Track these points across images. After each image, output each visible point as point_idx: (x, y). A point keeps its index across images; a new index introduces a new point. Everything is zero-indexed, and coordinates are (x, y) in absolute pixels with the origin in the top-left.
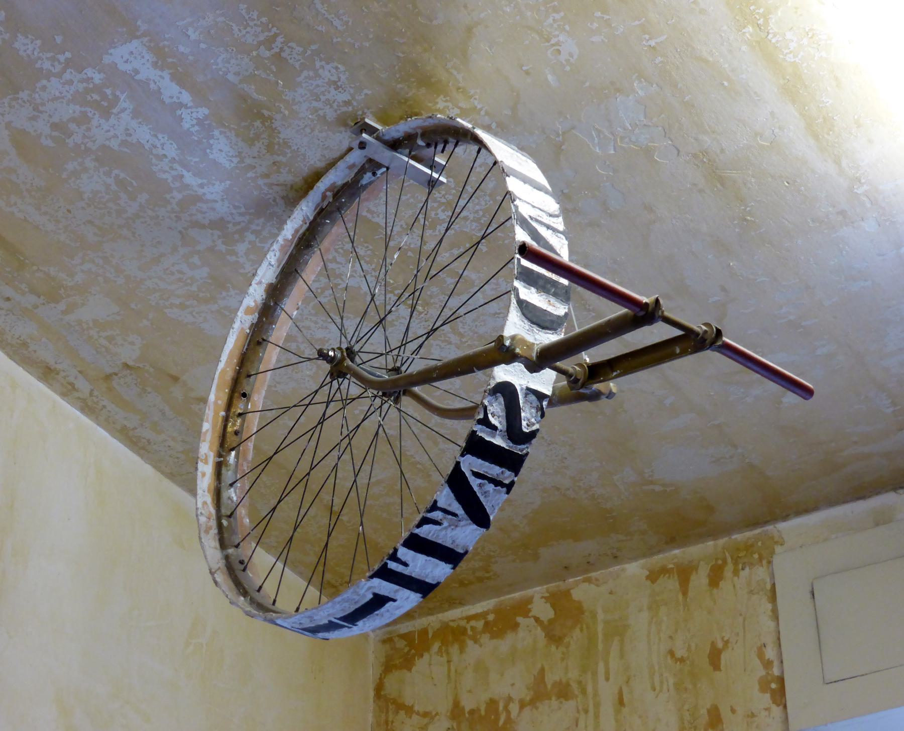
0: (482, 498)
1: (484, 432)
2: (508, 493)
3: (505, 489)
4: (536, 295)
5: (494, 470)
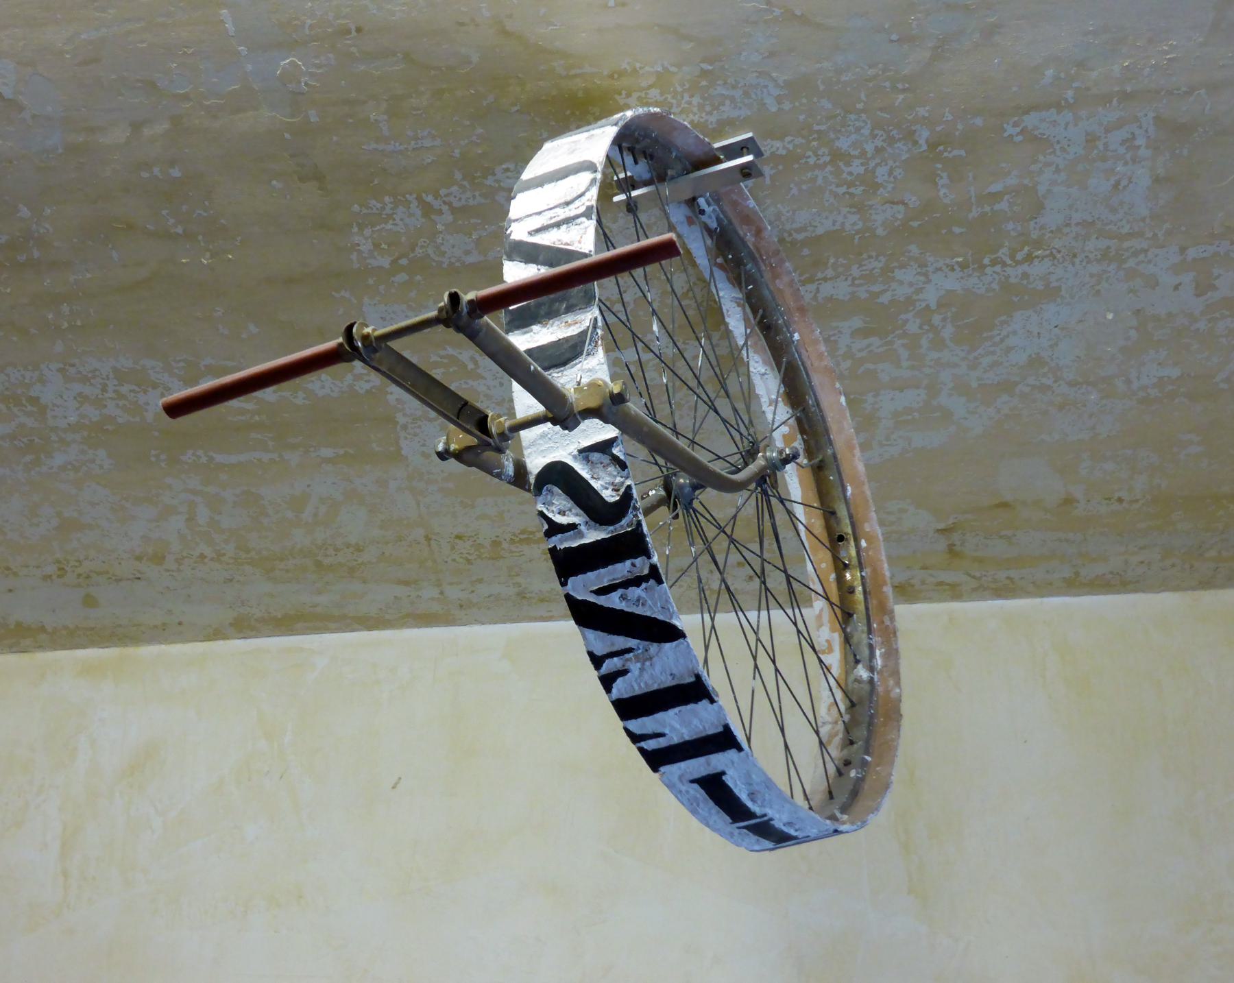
0: (639, 611)
1: (566, 540)
2: (660, 582)
3: (652, 582)
4: (545, 330)
5: (622, 570)
